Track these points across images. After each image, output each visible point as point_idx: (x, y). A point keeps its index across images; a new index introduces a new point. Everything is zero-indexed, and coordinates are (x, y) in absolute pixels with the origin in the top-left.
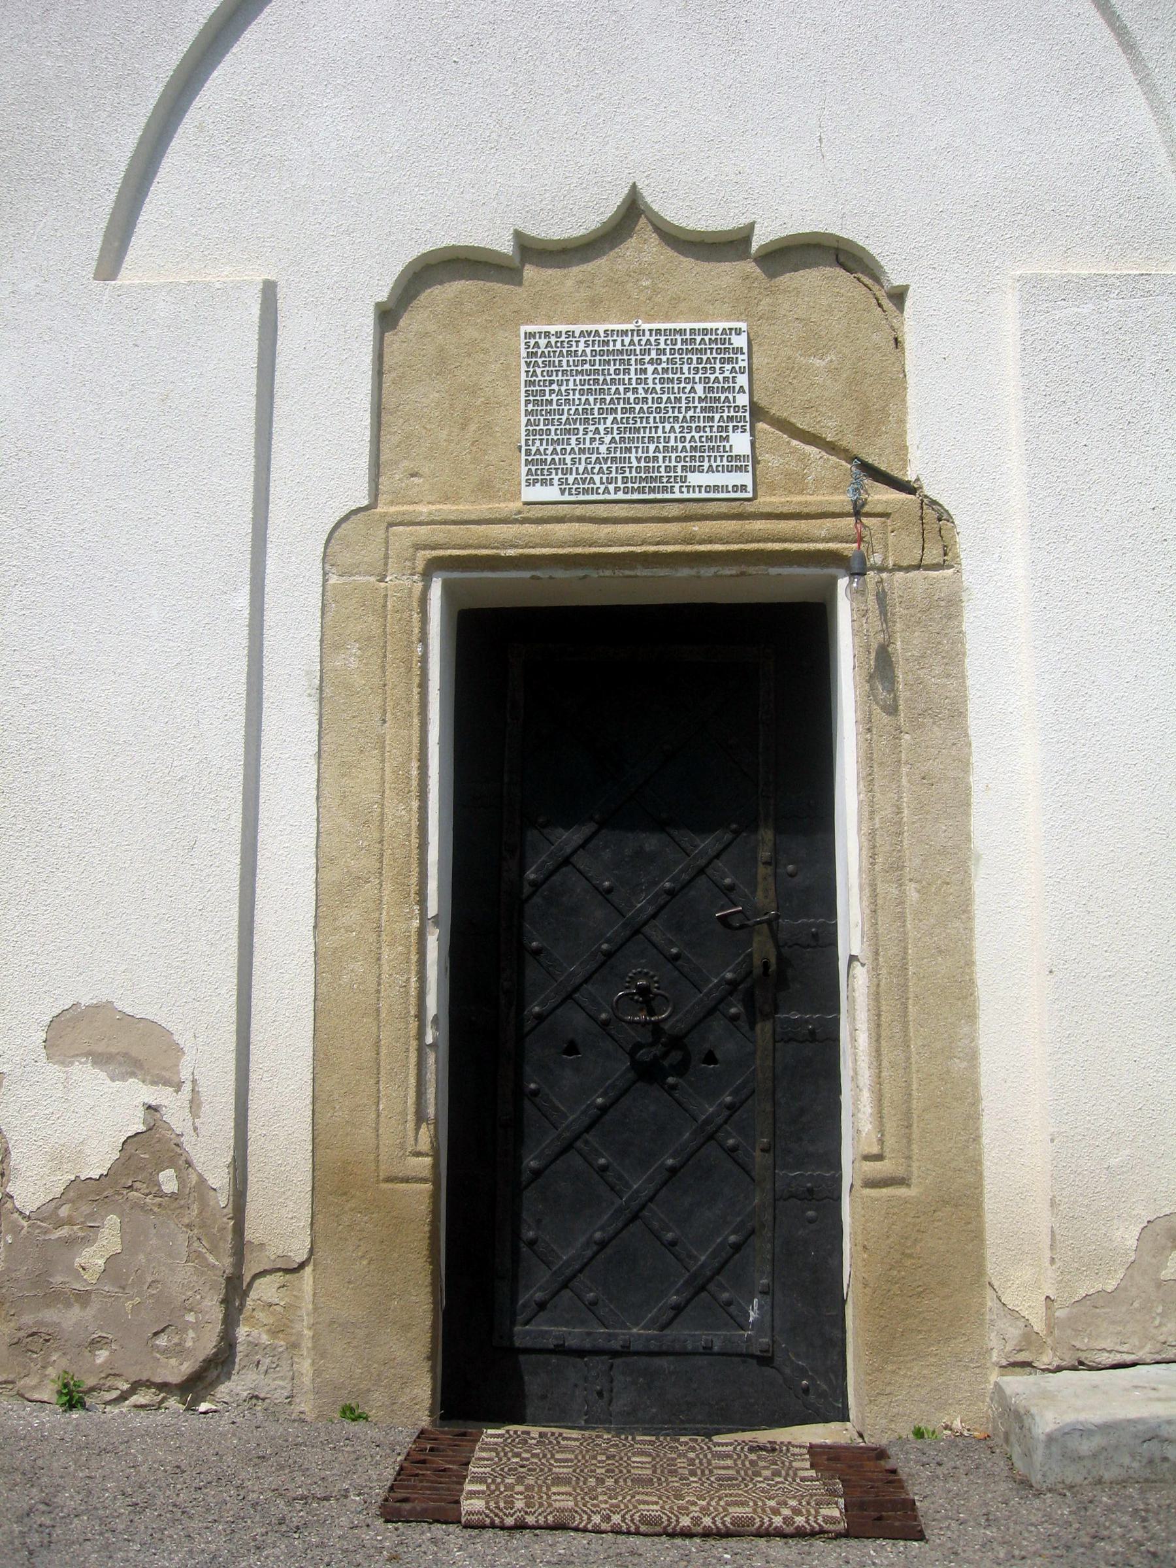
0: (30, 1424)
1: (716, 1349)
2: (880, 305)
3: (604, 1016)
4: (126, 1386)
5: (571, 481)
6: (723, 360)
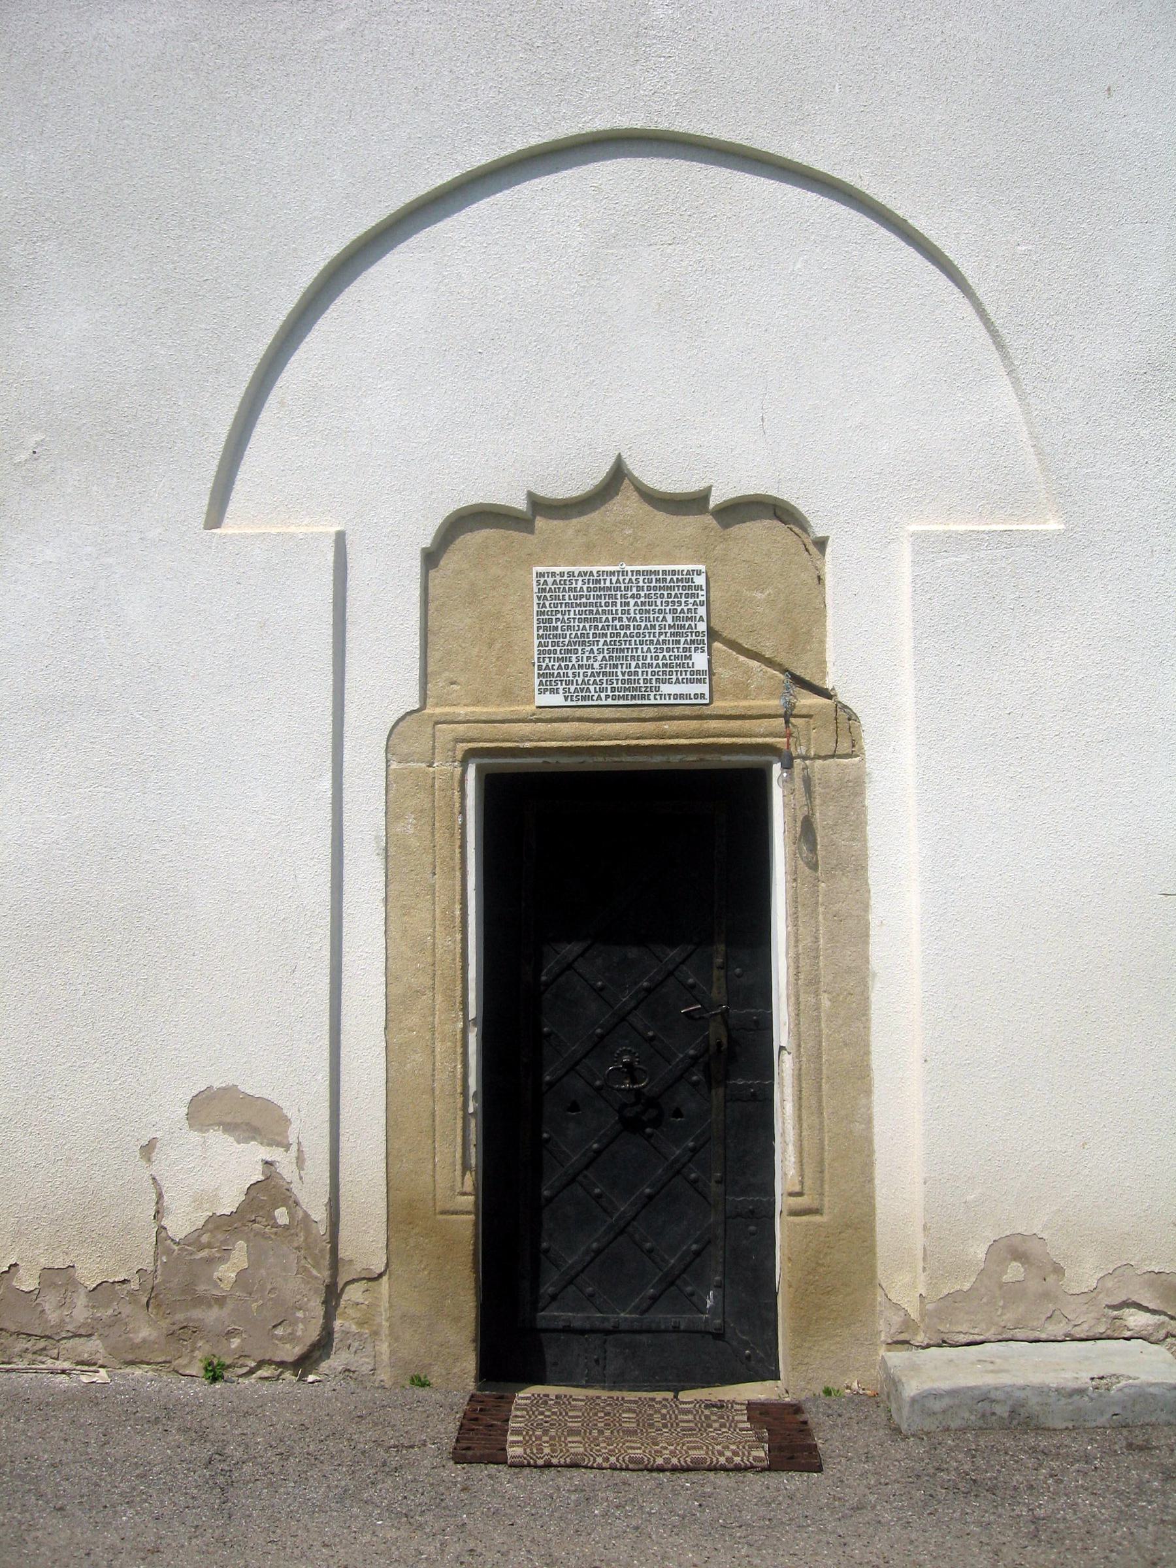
0: (187, 1393)
1: (682, 1327)
2: (807, 550)
3: (598, 1083)
4: (253, 1364)
5: (572, 690)
6: (687, 596)
